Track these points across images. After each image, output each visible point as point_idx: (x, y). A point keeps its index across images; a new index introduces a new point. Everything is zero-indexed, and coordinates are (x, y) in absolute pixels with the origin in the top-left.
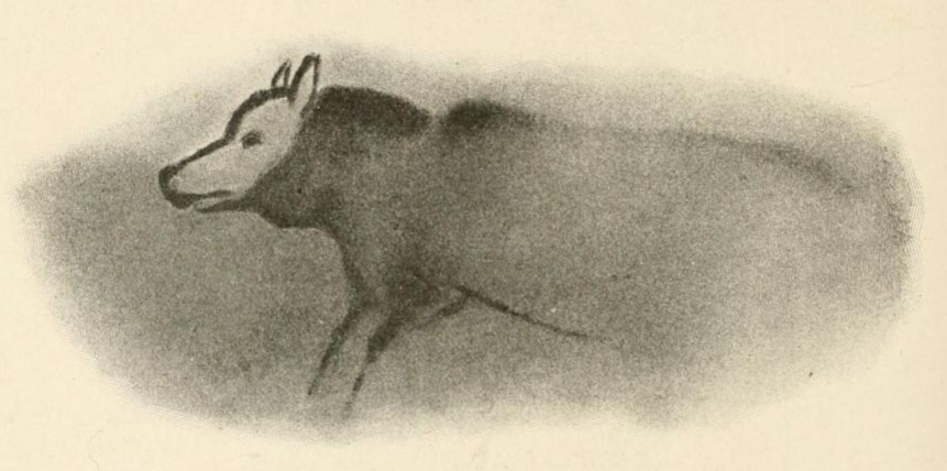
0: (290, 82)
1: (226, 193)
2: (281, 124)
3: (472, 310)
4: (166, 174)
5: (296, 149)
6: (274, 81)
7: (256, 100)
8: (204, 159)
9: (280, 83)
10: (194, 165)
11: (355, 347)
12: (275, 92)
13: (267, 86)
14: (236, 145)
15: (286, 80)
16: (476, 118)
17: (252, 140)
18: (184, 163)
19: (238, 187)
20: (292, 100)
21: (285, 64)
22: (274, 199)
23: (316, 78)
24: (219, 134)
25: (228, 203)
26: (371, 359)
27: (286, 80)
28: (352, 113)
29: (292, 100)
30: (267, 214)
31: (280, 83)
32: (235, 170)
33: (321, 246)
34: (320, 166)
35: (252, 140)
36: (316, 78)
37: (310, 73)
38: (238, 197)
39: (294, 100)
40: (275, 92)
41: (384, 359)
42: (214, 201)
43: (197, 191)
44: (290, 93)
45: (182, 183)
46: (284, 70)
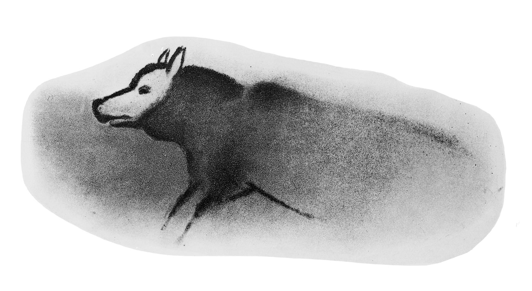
0: (168, 61)
1: (128, 117)
2: (160, 83)
3: (256, 196)
4: (97, 103)
5: (167, 97)
6: (159, 60)
7: (149, 69)
8: (117, 98)
9: (163, 60)
10: (110, 100)
11: (190, 207)
12: (159, 66)
13: (156, 62)
14: (136, 91)
15: (166, 58)
16: (272, 95)
17: (144, 90)
18: (106, 98)
19: (134, 113)
20: (168, 71)
21: (167, 50)
22: (150, 122)
23: (183, 60)
24: (127, 85)
25: (126, 123)
26: (196, 215)
27: (166, 58)
28: (198, 82)
29: (168, 71)
30: (151, 132)
31: (163, 60)
32: (135, 104)
33: (174, 152)
34: (181, 106)
35: (144, 90)
36: (183, 60)
37: (180, 56)
38: (133, 120)
39: (169, 71)
40: (159, 66)
41: (172, 219)
42: (121, 120)
43: (113, 114)
44: (167, 67)
45: (104, 109)
46: (166, 53)
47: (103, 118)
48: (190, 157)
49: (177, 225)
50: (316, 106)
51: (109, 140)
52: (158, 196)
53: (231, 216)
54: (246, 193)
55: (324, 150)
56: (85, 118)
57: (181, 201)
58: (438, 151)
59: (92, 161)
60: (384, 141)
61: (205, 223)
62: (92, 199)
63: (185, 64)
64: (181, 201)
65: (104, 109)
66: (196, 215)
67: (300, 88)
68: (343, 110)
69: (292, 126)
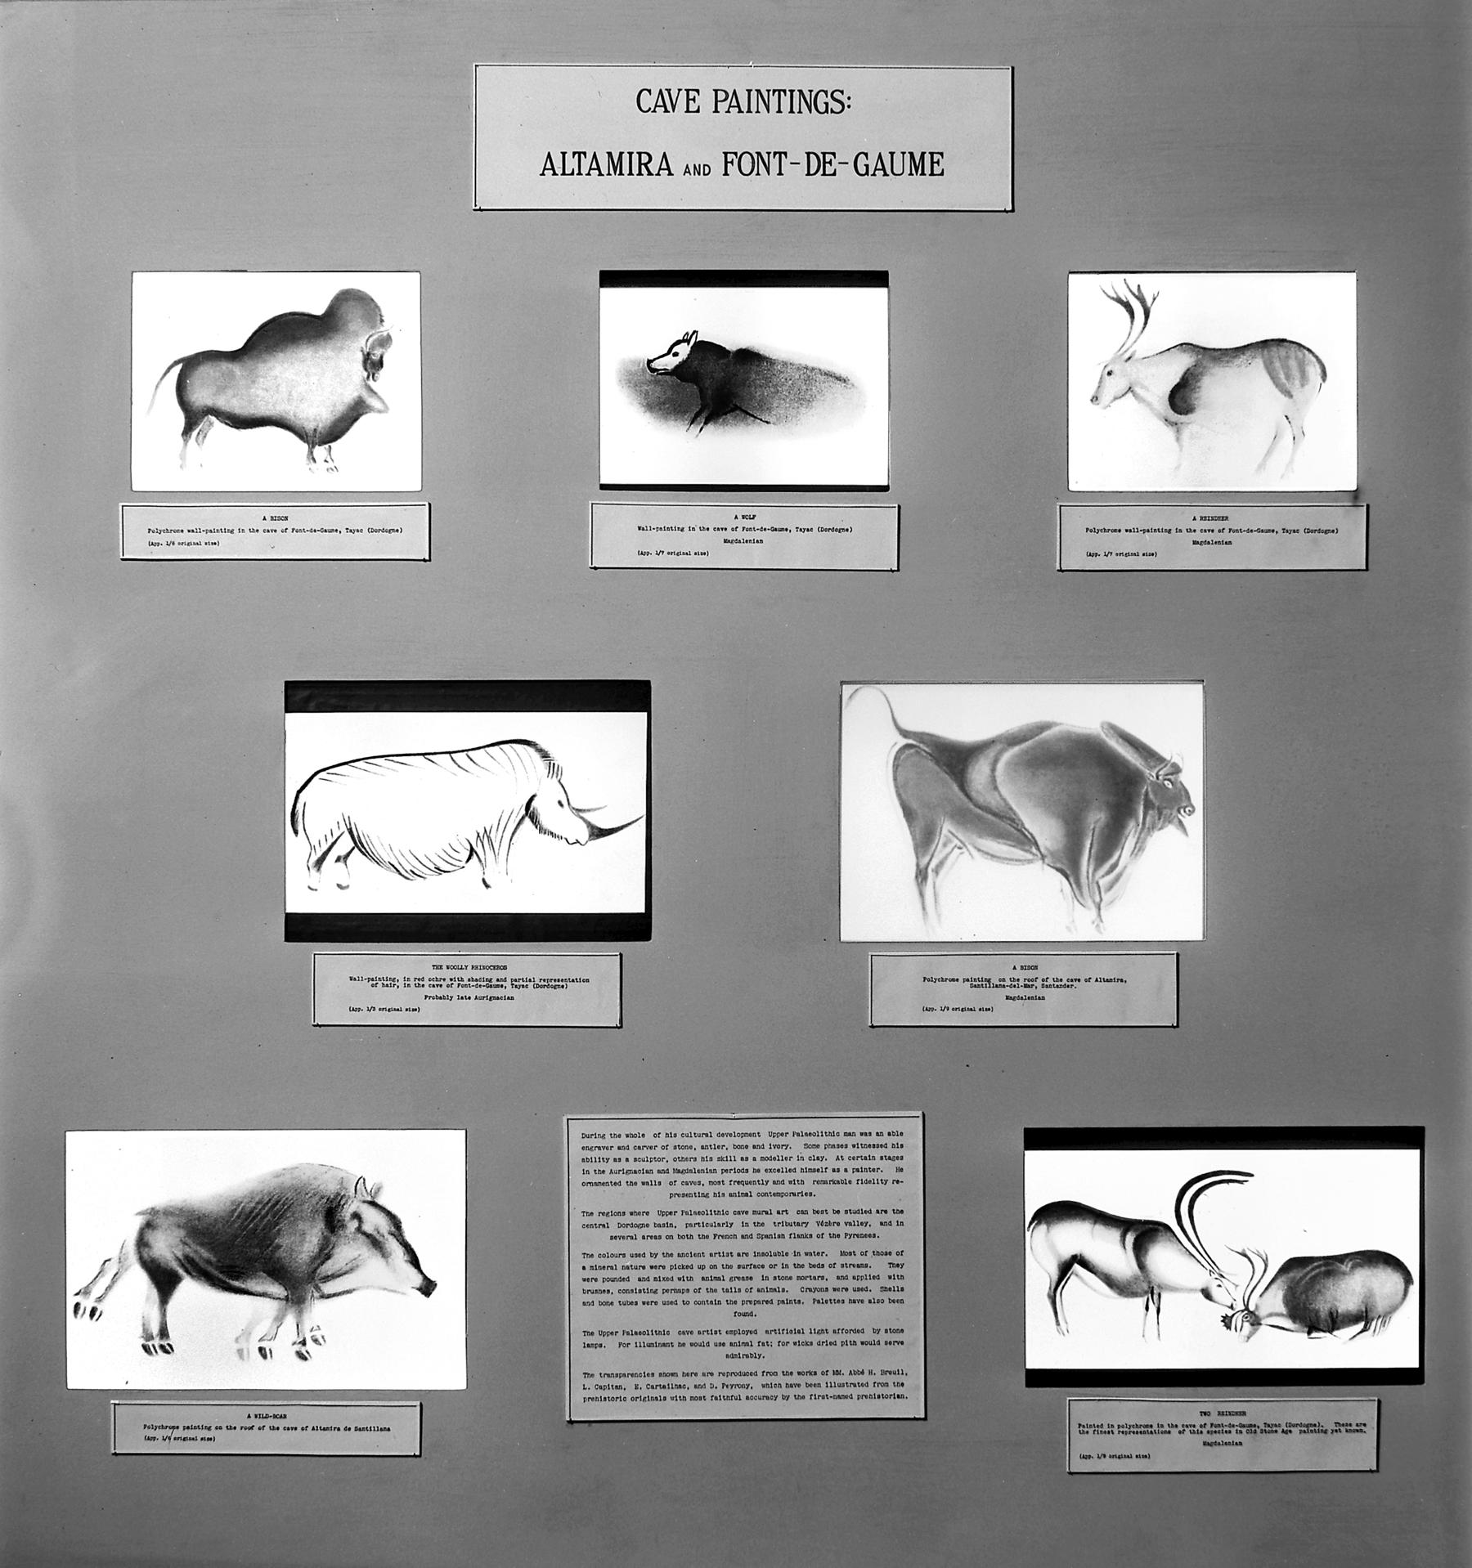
2: (684, 350)
4: (650, 362)
7: (678, 343)
16: (748, 357)
17: (676, 354)
22: (679, 371)
25: (666, 373)
28: (705, 350)
32: (671, 362)
35: (676, 354)
44: (688, 341)
45: (653, 365)
47: (653, 370)
48: (701, 391)
49: (695, 429)
50: (771, 362)
51: (657, 382)
52: (685, 412)
53: (725, 423)
54: (732, 410)
55: (775, 386)
56: (643, 371)
57: (697, 415)
58: (839, 385)
59: (647, 393)
60: (808, 380)
61: (710, 427)
62: (648, 414)
63: (1283, 1309)
64: (697, 415)
65: (653, 365)
66: (706, 423)
67: (329, 353)
68: (785, 364)
69: (757, 373)
